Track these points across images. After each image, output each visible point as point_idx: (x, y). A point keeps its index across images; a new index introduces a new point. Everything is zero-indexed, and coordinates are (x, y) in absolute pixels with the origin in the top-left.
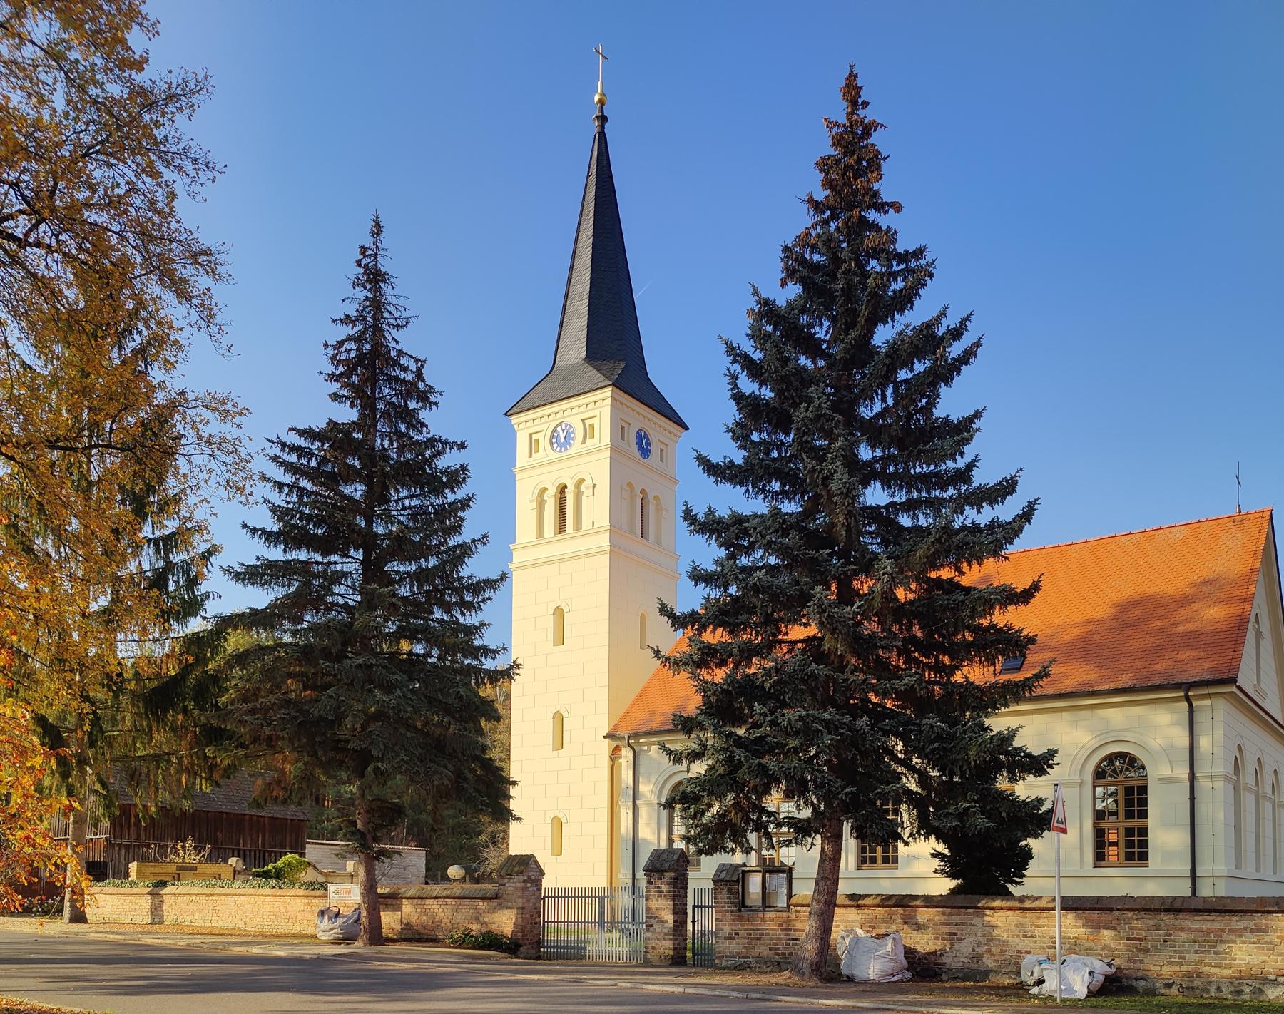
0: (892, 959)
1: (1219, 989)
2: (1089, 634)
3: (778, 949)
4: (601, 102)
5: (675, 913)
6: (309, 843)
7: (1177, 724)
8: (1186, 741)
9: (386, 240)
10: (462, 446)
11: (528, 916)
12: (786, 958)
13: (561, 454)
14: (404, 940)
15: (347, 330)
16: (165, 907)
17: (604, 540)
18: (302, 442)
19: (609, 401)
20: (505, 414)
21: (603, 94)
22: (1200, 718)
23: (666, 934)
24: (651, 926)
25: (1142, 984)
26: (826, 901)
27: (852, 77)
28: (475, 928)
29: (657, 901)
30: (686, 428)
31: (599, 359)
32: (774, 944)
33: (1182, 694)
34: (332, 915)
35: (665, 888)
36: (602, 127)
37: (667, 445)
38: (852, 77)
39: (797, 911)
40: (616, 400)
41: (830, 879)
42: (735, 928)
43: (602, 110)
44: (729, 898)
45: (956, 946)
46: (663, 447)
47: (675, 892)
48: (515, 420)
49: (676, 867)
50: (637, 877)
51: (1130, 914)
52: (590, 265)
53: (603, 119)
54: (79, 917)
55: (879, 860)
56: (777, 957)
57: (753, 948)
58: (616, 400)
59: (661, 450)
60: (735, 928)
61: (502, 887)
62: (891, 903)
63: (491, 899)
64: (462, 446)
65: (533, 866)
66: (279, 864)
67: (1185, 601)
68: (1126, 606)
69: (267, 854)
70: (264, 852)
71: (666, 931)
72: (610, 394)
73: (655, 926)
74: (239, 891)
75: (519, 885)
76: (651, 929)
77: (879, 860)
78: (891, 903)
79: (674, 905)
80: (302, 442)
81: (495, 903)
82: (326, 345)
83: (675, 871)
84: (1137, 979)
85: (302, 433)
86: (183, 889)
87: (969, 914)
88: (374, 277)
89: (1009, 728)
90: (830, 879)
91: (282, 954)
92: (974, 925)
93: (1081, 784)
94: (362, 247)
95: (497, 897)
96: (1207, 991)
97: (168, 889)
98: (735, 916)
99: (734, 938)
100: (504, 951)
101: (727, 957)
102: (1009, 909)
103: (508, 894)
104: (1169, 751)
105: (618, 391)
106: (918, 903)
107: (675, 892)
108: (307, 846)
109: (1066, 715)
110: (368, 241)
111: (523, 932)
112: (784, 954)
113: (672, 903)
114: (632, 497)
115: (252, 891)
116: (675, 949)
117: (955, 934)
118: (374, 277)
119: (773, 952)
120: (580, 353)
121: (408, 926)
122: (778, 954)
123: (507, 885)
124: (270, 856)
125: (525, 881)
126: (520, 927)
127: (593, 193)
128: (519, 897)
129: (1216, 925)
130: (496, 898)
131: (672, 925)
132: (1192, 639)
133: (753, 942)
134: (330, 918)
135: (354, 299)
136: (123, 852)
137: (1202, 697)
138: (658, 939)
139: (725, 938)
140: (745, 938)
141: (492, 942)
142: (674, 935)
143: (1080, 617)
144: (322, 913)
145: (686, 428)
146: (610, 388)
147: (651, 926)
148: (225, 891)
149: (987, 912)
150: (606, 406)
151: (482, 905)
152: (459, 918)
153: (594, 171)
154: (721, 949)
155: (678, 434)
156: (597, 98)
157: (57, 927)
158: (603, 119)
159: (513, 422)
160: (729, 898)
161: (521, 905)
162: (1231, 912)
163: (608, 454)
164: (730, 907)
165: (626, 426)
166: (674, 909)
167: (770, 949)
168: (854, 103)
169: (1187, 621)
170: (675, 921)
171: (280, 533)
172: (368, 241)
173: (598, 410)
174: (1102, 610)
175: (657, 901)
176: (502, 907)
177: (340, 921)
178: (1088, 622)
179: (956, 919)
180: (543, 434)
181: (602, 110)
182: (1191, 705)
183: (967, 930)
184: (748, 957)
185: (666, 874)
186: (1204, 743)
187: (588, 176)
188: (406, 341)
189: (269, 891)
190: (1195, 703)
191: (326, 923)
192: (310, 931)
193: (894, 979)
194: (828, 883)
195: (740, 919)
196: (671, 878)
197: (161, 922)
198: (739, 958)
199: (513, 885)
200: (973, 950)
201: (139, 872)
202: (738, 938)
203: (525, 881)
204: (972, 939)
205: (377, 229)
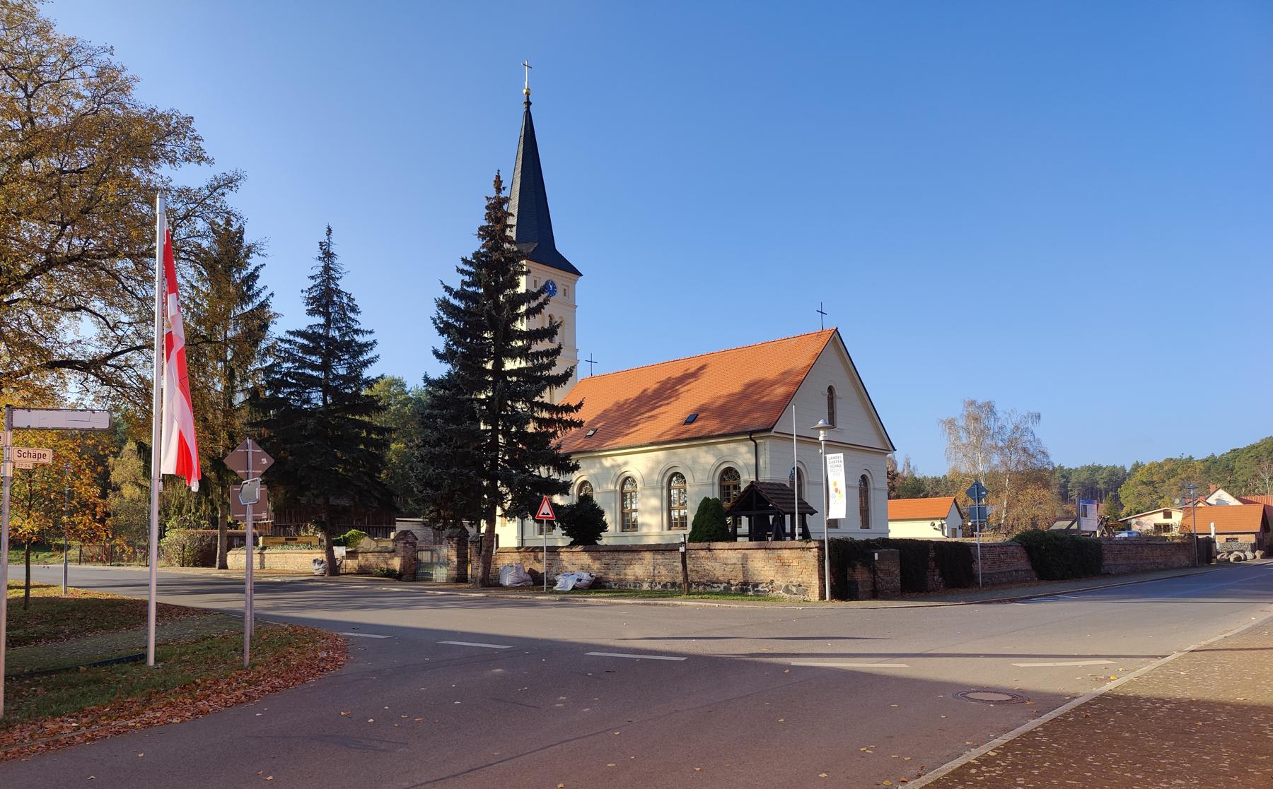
1: (630, 585)
2: (728, 402)
4: (528, 94)
7: (749, 452)
8: (753, 461)
9: (334, 238)
10: (371, 332)
11: (407, 560)
14: (517, 588)
15: (312, 283)
16: (266, 560)
18: (292, 338)
21: (528, 89)
22: (761, 449)
25: (608, 584)
27: (498, 177)
28: (384, 566)
30: (581, 275)
31: (523, 243)
33: (748, 437)
34: (320, 562)
35: (454, 545)
36: (528, 108)
37: (568, 286)
38: (498, 177)
51: (605, 553)
53: (528, 103)
54: (224, 566)
59: (564, 290)
62: (529, 550)
63: (391, 552)
64: (371, 332)
66: (347, 535)
67: (773, 383)
68: (749, 386)
69: (371, 529)
70: (369, 527)
75: (402, 545)
78: (529, 550)
80: (292, 338)
81: (393, 554)
82: (302, 291)
83: (458, 537)
84: (606, 582)
86: (273, 551)
88: (328, 255)
89: (951, 423)
91: (279, 580)
93: (713, 484)
94: (320, 243)
96: (626, 586)
97: (268, 551)
102: (567, 552)
104: (746, 465)
109: (704, 448)
110: (324, 238)
111: (404, 568)
118: (328, 255)
121: (360, 567)
124: (373, 530)
125: (404, 543)
126: (403, 566)
129: (630, 557)
132: (763, 407)
134: (318, 564)
135: (318, 268)
136: (282, 530)
137: (761, 438)
141: (390, 574)
143: (726, 392)
148: (290, 551)
149: (561, 554)
151: (387, 555)
156: (525, 91)
157: (214, 572)
158: (528, 103)
162: (619, 551)
165: (538, 280)
168: (499, 190)
169: (766, 396)
171: (231, 405)
172: (324, 238)
174: (736, 388)
177: (323, 565)
178: (730, 395)
182: (756, 443)
186: (761, 462)
188: (343, 285)
189: (307, 551)
190: (757, 441)
191: (317, 566)
192: (309, 570)
193: (518, 585)
197: (264, 568)
201: (264, 542)
203: (404, 543)
205: (330, 231)
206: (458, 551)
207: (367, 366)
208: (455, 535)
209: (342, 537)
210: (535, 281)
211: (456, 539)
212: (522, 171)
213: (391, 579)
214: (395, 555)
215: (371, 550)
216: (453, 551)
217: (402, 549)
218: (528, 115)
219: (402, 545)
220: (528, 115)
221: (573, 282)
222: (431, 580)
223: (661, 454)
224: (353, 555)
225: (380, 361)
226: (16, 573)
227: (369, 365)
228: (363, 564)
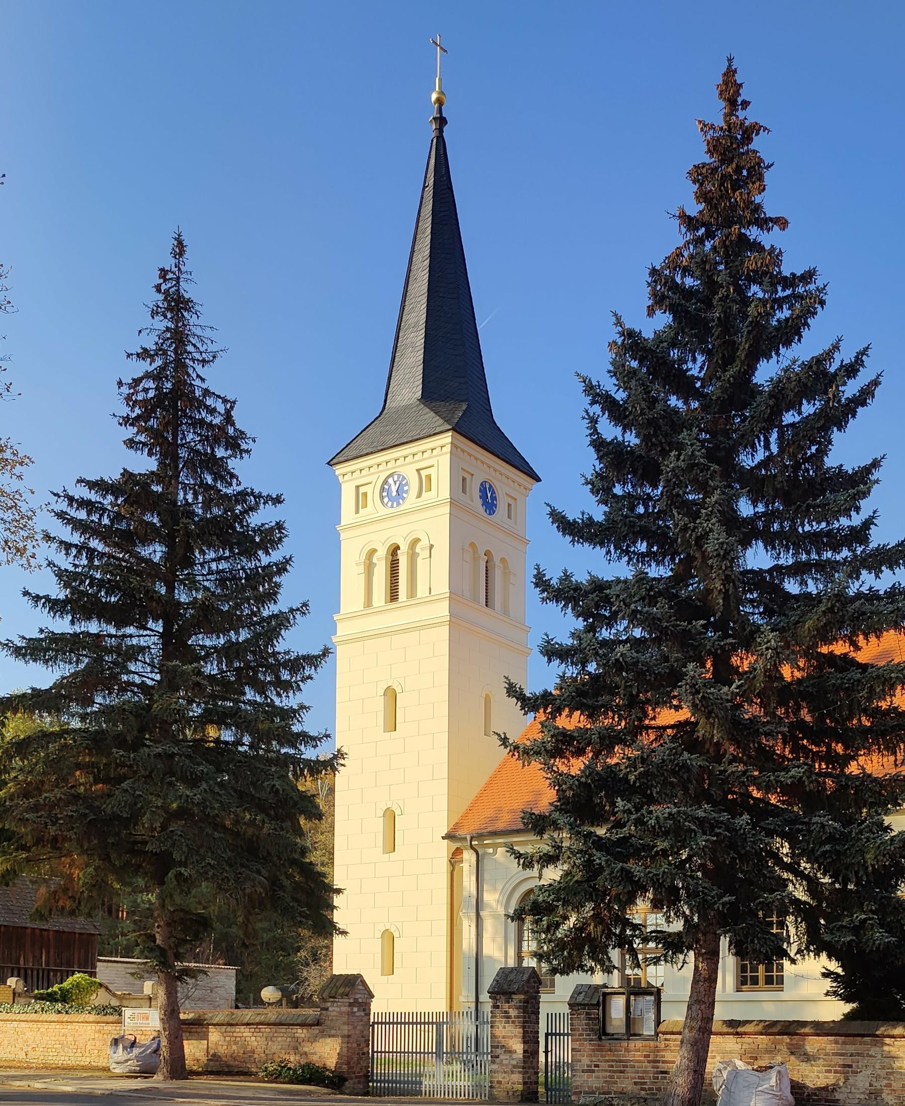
0: (777, 1096)
3: (645, 1083)
4: (440, 102)
5: (524, 1042)
6: (101, 961)
9: (190, 261)
10: (278, 500)
11: (355, 1045)
12: (654, 1094)
13: (392, 510)
15: (145, 366)
17: (442, 610)
18: (93, 496)
19: (448, 449)
20: (328, 463)
21: (441, 92)
22: (487, 864)
23: (514, 1067)
24: (497, 1057)
26: (700, 1028)
27: (730, 73)
28: (293, 1059)
29: (504, 1027)
32: (639, 1078)
34: (127, 1044)
35: (513, 1013)
36: (440, 130)
37: (515, 499)
38: (730, 73)
39: (666, 1040)
40: (457, 447)
41: (704, 1003)
42: (594, 1059)
43: (440, 110)
44: (587, 1024)
45: (851, 1080)
46: (511, 502)
47: (524, 1017)
48: (339, 470)
49: (526, 989)
50: (480, 1000)
53: (441, 121)
55: (761, 980)
56: (643, 1092)
57: (616, 1083)
58: (457, 447)
59: (509, 505)
60: (594, 1059)
61: (324, 1012)
62: (775, 1030)
63: (311, 1025)
64: (278, 500)
65: (361, 987)
66: (66, 985)
69: (52, 974)
70: (49, 971)
71: (514, 1062)
72: (449, 440)
73: (501, 1057)
74: (19, 1017)
75: (345, 1009)
76: (497, 1060)
77: (761, 980)
78: (775, 1030)
79: (524, 1032)
80: (93, 496)
81: (316, 1030)
82: (120, 384)
83: (525, 993)
85: (92, 485)
87: (865, 1043)
90: (704, 1003)
92: (871, 1056)
94: (162, 270)
95: (318, 1023)
98: (594, 1045)
99: (593, 1071)
100: (326, 1086)
101: (586, 1093)
103: (331, 1020)
106: (807, 1030)
107: (524, 1017)
108: (98, 964)
111: (348, 1063)
112: (650, 1089)
113: (521, 1030)
114: (475, 559)
115: (34, 1016)
116: (525, 1083)
117: (850, 1066)
119: (639, 1087)
120: (415, 393)
121: (215, 1057)
122: (642, 1089)
123: (330, 1009)
124: (55, 975)
125: (351, 1005)
126: (344, 1058)
128: (344, 1024)
130: (318, 1024)
131: (521, 1056)
133: (616, 1075)
134: (125, 1048)
138: (505, 1072)
139: (583, 1071)
140: (606, 1071)
142: (524, 1068)
144: (116, 1042)
147: (497, 1057)
149: (887, 1040)
150: (446, 453)
151: (301, 1033)
152: (274, 1047)
153: (431, 181)
154: (578, 1083)
156: (434, 96)
158: (441, 121)
160: (587, 1024)
161: (346, 1033)
163: (447, 509)
164: (589, 1035)
166: (524, 1037)
167: (636, 1083)
170: (525, 1052)
171: (67, 601)
172: (169, 263)
173: (436, 459)
175: (504, 1027)
176: (324, 1034)
177: (136, 1051)
179: (851, 1048)
181: (440, 110)
183: (863, 1062)
184: (610, 1093)
185: (514, 996)
187: (424, 187)
189: (54, 1017)
191: (120, 1053)
194: (703, 1007)
195: (600, 1049)
196: (520, 1002)
198: (600, 1094)
199: (337, 1009)
200: (871, 1085)
202: (598, 1071)
203: (351, 1005)
204: (869, 1072)
205: (180, 249)
207: (36, 662)
208: (516, 986)
209: (56, 988)
210: (464, 479)
213: (325, 1090)
214: (322, 1031)
215: (246, 1021)
217: (345, 1019)
218: (440, 142)
219: (345, 1009)
220: (440, 142)
222: (419, 1093)
224: (194, 1029)
227: (288, 567)
228: (222, 1050)
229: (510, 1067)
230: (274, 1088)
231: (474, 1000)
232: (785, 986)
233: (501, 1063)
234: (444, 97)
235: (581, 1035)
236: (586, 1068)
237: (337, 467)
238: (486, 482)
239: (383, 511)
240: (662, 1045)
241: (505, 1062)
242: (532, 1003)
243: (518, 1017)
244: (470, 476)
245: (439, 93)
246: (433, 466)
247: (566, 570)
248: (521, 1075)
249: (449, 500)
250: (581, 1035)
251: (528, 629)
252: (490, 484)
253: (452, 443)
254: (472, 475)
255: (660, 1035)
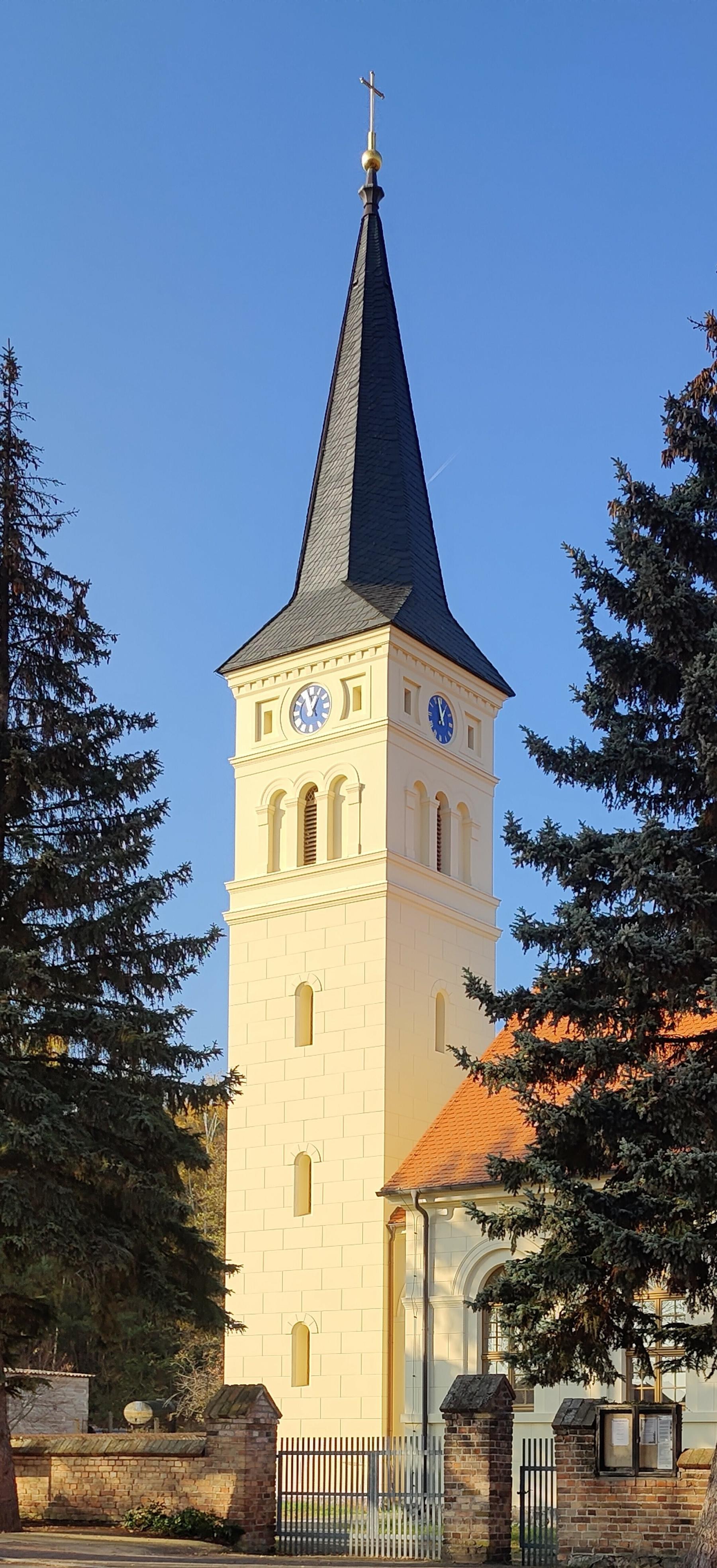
4: (373, 165)
5: (491, 1480)
10: (147, 722)
11: (255, 1484)
12: (671, 1552)
13: (306, 737)
17: (377, 875)
19: (384, 650)
20: (218, 671)
21: (376, 153)
23: (478, 1514)
24: (454, 1500)
28: (169, 1504)
30: (511, 694)
35: (475, 1438)
36: (374, 205)
37: (479, 721)
39: (689, 1476)
40: (397, 648)
44: (578, 1455)
46: (473, 724)
47: (491, 1445)
48: (234, 680)
50: (430, 1421)
52: (354, 428)
53: (375, 193)
56: (657, 1550)
58: (397, 648)
59: (470, 729)
64: (147, 722)
71: (477, 1508)
72: (387, 638)
73: (459, 1500)
75: (241, 1433)
81: (201, 1462)
83: (493, 1411)
105: (395, 628)
107: (491, 1445)
113: (487, 1463)
114: (423, 805)
116: (492, 1537)
120: (338, 572)
121: (60, 1501)
125: (249, 1427)
127: (360, 312)
131: (487, 1499)
138: (465, 1522)
142: (490, 1515)
145: (511, 694)
146: (387, 629)
147: (454, 1500)
150: (382, 657)
151: (180, 1466)
152: (143, 1487)
153: (361, 277)
155: (497, 702)
156: (365, 158)
158: (375, 193)
159: (231, 684)
160: (578, 1455)
163: (383, 735)
164: (581, 1469)
165: (412, 689)
170: (492, 1493)
173: (369, 664)
176: (212, 1469)
180: (280, 701)
185: (477, 1416)
187: (352, 285)
203: (249, 1427)
206: (490, 1459)
208: (479, 1402)
211: (483, 1417)
212: (363, 381)
213: (214, 1547)
216: (471, 1459)
217: (241, 1447)
219: (241, 1433)
221: (491, 710)
223: (437, 1263)
225: (172, 809)
226: (8, 1280)
227: (162, 815)
228: (70, 1491)
229: (472, 1514)
230: (143, 1543)
231: (421, 1421)
232: (535, 1405)
233: (459, 1509)
234: (379, 159)
235: (570, 1469)
236: (577, 1515)
237: (230, 676)
238: (437, 697)
239: (294, 737)
240: (684, 1484)
241: (464, 1507)
242: (502, 1425)
243: (483, 1444)
244: (416, 688)
245: (372, 154)
246: (363, 675)
247: (549, 820)
248: (487, 1526)
249: (386, 722)
250: (570, 1469)
251: (497, 903)
252: (443, 700)
253: (390, 642)
254: (419, 687)
255: (681, 1469)
